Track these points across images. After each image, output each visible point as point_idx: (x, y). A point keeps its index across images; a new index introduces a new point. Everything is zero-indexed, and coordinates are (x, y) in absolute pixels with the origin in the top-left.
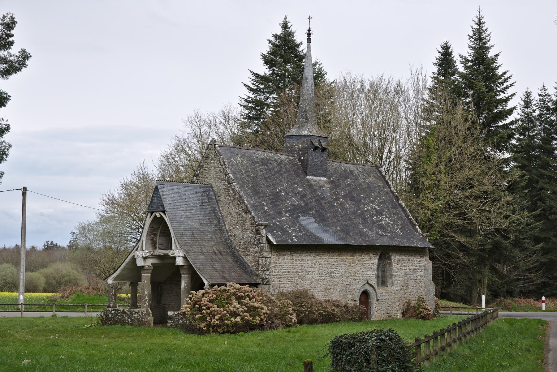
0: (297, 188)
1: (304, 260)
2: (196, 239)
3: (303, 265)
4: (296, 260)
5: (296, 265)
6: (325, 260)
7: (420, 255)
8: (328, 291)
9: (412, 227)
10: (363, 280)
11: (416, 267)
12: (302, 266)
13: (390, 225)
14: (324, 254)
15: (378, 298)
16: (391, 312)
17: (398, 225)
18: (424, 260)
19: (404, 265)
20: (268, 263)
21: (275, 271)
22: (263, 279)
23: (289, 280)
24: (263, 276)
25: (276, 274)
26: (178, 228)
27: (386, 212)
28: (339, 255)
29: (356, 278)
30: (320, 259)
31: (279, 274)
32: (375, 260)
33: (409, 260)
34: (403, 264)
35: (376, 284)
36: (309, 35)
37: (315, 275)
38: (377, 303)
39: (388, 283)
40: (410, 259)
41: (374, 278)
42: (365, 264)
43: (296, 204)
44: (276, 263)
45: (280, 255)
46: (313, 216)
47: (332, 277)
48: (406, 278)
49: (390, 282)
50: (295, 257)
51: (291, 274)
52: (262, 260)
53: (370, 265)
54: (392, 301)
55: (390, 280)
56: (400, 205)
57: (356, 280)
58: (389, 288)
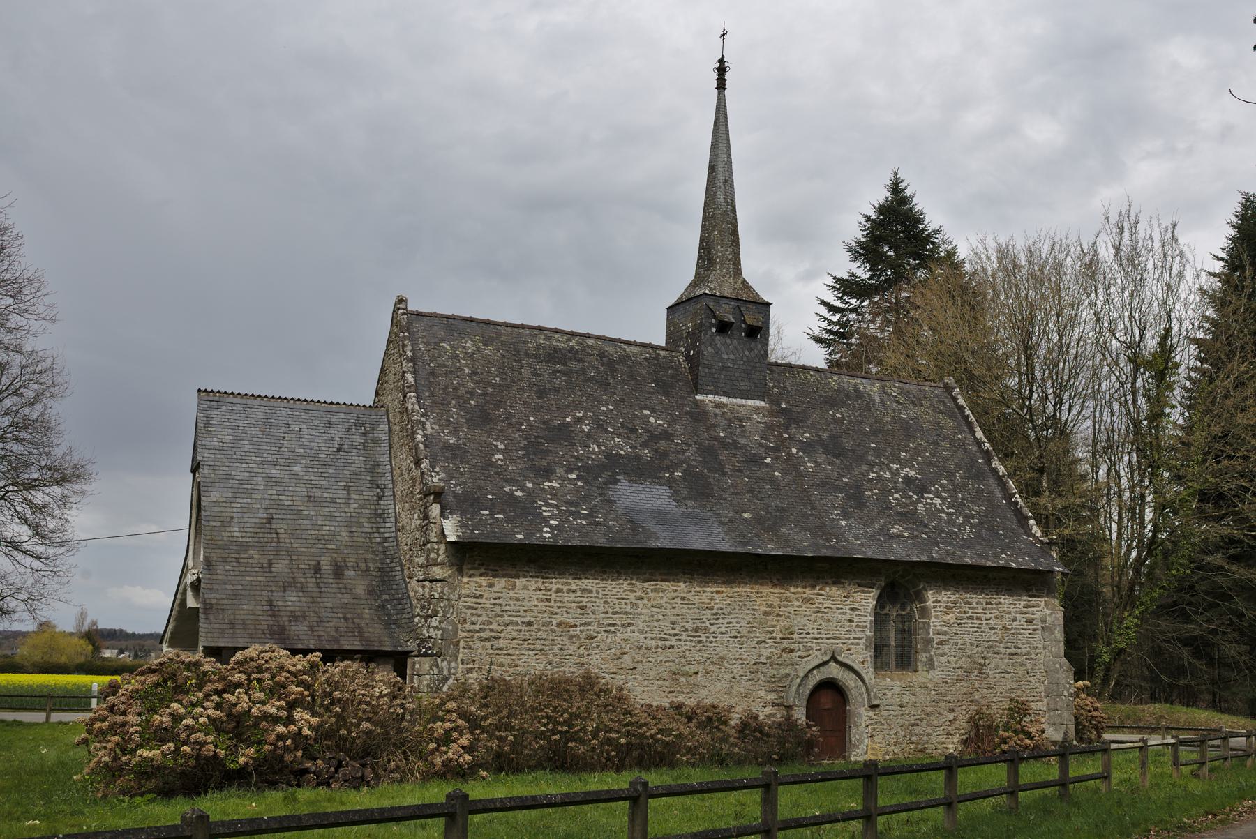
0: (648, 417)
1: (591, 592)
2: (275, 536)
3: (588, 605)
4: (558, 591)
5: (559, 604)
6: (674, 594)
7: (1028, 590)
8: (683, 680)
9: (1019, 522)
10: (818, 653)
11: (1014, 620)
12: (582, 608)
13: (944, 516)
14: (671, 578)
15: (876, 702)
16: (925, 738)
17: (968, 517)
18: (1043, 604)
19: (970, 614)
20: (435, 594)
21: (474, 619)
22: (424, 641)
23: (532, 647)
24: (425, 631)
25: (477, 627)
26: (224, 504)
27: (942, 485)
28: (727, 583)
29: (792, 646)
30: (654, 591)
31: (491, 627)
32: (867, 600)
34: (965, 613)
35: (869, 663)
36: (722, 70)
37: (636, 634)
38: (871, 714)
39: (919, 664)
40: (994, 601)
42: (826, 610)
43: (622, 452)
44: (481, 596)
45: (495, 576)
46: (671, 483)
47: (700, 642)
48: (979, 649)
49: (924, 659)
50: (556, 583)
51: (539, 630)
52: (423, 587)
53: (845, 613)
54: (929, 710)
55: (924, 655)
56: (995, 471)
57: (792, 651)
58: (922, 676)
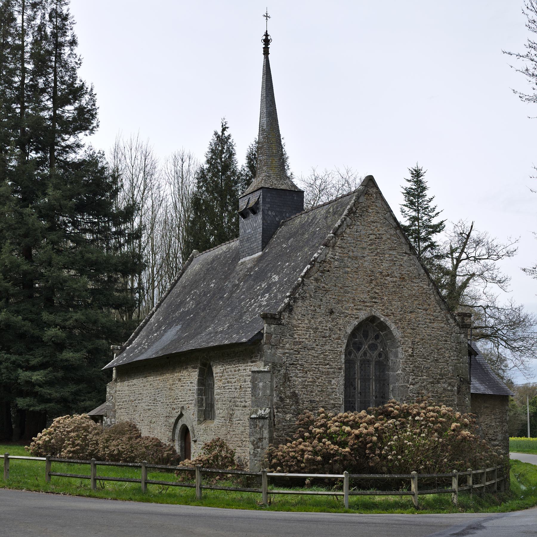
33: (235, 371)
36: (267, 42)
41: (193, 405)
42: (183, 385)
